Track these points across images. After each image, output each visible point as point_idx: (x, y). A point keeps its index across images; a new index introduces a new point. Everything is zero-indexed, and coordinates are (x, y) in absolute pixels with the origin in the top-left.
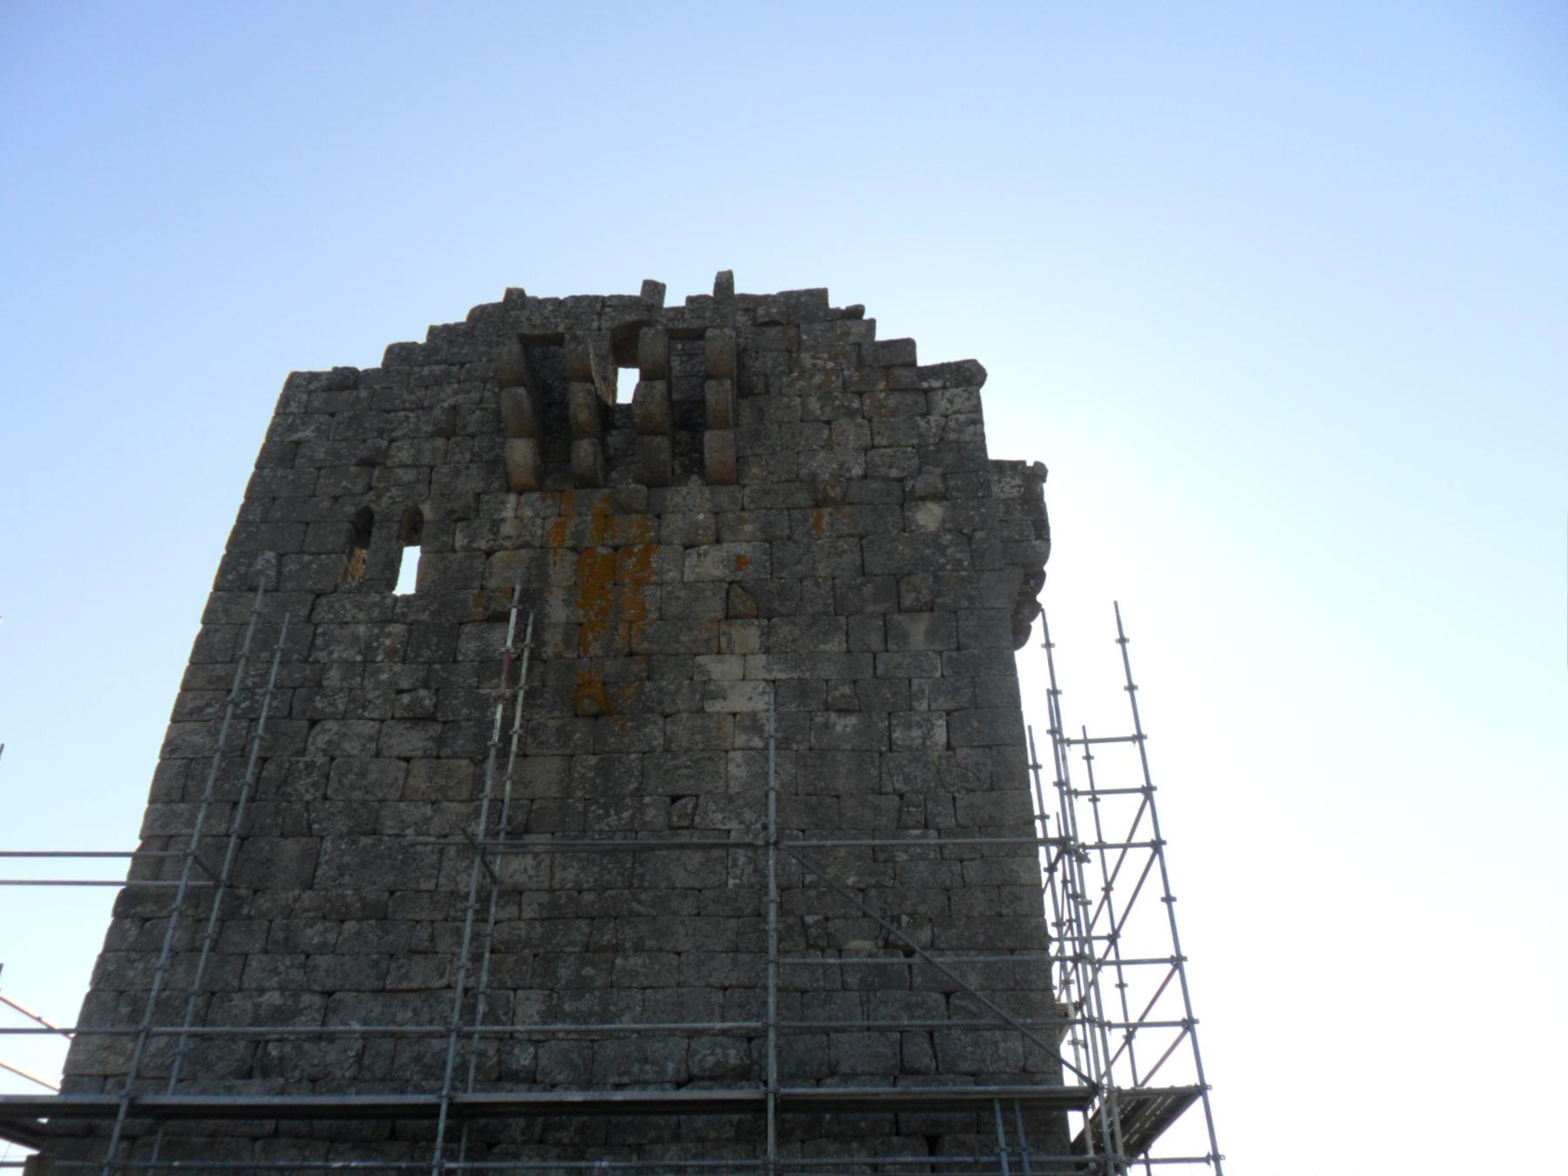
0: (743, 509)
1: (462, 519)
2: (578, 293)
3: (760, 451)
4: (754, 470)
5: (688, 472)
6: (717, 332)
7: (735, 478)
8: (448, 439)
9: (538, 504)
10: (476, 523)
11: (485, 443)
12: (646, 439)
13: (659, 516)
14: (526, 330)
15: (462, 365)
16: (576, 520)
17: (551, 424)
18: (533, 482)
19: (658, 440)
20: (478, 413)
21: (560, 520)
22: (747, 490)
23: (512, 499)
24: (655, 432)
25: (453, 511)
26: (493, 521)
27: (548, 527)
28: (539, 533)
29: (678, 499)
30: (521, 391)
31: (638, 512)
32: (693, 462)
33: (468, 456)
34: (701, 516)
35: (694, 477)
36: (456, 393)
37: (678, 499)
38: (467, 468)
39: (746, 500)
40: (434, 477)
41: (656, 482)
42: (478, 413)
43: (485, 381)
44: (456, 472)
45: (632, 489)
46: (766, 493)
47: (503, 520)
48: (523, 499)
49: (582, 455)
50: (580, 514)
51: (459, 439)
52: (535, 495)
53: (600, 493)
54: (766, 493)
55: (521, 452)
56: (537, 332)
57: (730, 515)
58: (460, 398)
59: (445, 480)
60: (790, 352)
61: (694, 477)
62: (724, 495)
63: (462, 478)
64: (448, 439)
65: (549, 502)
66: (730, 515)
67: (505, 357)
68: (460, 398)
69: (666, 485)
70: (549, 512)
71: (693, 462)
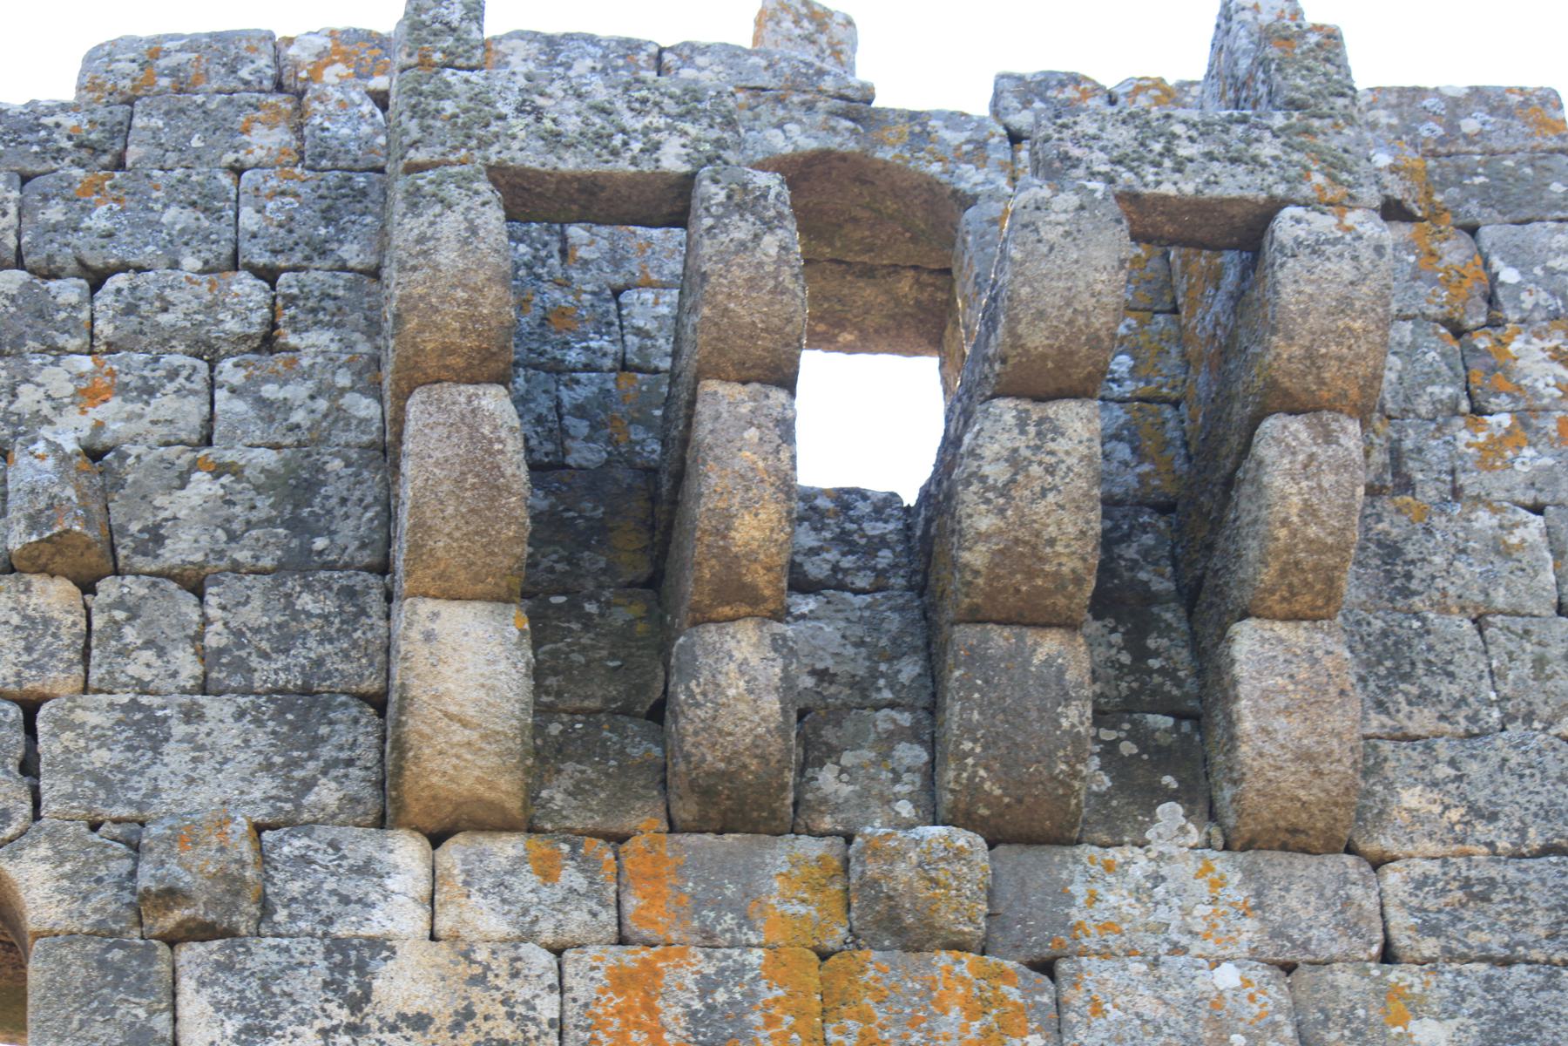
0: (1388, 955)
1: (202, 932)
2: (146, 28)
3: (1422, 720)
4: (1412, 798)
5: (1136, 792)
6: (1324, 223)
7: (1334, 832)
8: (87, 587)
9: (526, 884)
10: (263, 954)
11: (253, 614)
12: (1000, 639)
13: (1046, 967)
14: (527, 155)
15: (96, 279)
16: (700, 963)
17: (614, 540)
18: (506, 790)
19: (1049, 645)
20: (203, 486)
21: (630, 957)
22: (1393, 878)
23: (405, 853)
24: (1032, 616)
25: (171, 896)
26: (338, 945)
27: (580, 988)
28: (548, 1007)
29: (1117, 899)
30: (495, 402)
31: (958, 945)
32: (1173, 743)
33: (188, 666)
34: (1227, 977)
35: (1170, 813)
36: (88, 395)
37: (1117, 899)
38: (192, 715)
39: (1400, 922)
40: (47, 746)
41: (1028, 826)
42: (203, 486)
43: (208, 352)
44: (146, 731)
45: (936, 858)
46: (1478, 893)
47: (380, 946)
48: (453, 853)
49: (735, 688)
50: (709, 940)
51: (134, 587)
52: (508, 848)
53: (785, 861)
54: (1478, 893)
55: (467, 664)
56: (570, 163)
57: (1343, 977)
58: (113, 416)
59: (100, 757)
60: (1458, 331)
61: (1170, 813)
62: (1304, 892)
63: (176, 756)
64: (87, 587)
65: (572, 877)
66: (1343, 977)
67: (447, 256)
68: (113, 416)
69: (1064, 837)
70: (577, 920)
71: (1173, 743)
